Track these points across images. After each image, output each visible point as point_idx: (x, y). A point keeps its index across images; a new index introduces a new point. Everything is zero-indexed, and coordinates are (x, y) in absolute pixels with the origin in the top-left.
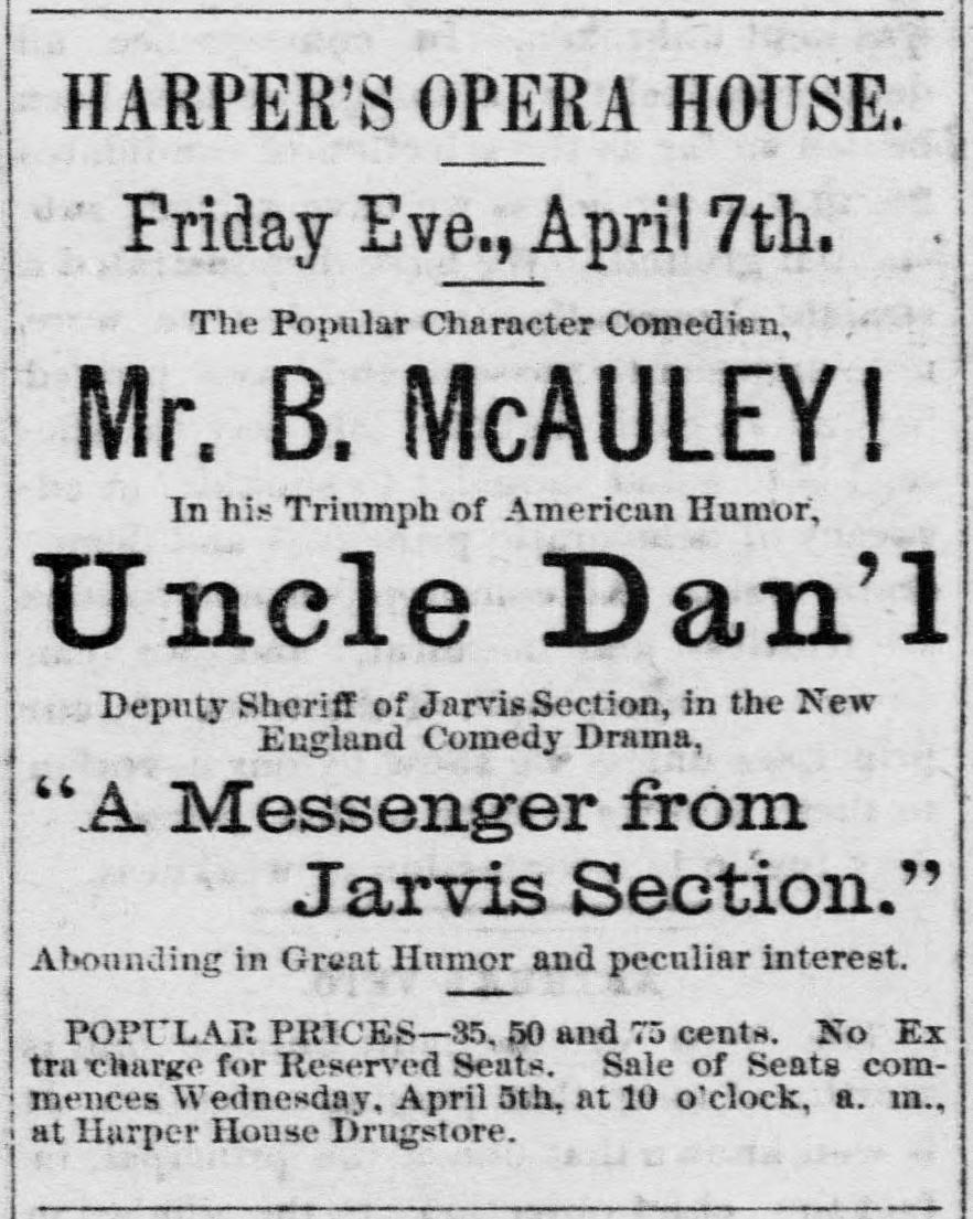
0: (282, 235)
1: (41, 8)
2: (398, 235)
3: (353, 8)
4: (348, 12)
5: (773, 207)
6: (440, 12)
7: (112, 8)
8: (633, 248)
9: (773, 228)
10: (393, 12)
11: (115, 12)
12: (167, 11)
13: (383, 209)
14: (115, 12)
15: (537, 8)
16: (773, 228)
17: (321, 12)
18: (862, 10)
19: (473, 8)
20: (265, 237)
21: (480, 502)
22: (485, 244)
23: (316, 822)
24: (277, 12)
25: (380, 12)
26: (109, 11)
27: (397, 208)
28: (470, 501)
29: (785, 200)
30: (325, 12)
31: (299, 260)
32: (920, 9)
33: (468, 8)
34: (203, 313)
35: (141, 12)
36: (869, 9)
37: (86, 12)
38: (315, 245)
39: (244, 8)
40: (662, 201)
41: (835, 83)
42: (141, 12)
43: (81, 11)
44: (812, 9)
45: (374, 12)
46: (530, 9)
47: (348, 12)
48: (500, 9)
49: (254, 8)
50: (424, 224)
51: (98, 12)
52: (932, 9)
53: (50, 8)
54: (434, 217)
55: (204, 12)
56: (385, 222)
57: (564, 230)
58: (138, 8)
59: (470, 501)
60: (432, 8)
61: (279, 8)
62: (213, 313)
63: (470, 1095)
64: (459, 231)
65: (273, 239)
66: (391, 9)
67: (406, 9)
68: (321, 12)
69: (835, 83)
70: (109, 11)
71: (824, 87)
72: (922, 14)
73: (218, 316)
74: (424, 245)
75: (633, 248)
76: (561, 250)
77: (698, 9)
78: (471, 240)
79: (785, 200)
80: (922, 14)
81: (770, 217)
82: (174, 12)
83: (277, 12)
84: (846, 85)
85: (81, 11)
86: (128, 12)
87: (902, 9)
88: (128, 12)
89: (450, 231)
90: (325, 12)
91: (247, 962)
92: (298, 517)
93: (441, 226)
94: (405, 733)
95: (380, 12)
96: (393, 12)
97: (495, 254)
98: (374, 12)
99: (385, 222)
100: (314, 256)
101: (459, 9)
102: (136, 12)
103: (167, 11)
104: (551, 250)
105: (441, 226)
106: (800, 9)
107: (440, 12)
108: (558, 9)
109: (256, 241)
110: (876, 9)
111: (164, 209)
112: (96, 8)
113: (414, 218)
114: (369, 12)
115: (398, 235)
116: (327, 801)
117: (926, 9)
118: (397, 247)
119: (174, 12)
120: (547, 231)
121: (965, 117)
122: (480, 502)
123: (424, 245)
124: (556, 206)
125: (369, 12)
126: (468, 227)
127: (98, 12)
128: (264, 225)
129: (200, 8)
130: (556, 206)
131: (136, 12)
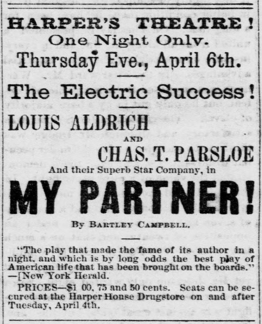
0: (85, 63)
1: (12, 319)
2: (116, 63)
3: (96, 319)
4: (95, 320)
5: (224, 56)
6: (119, 320)
7: (31, 319)
8: (183, 66)
9: (224, 61)
10: (107, 320)
11: (32, 320)
12: (46, 320)
13: (113, 56)
14: (32, 320)
15: (146, 319)
16: (224, 61)
17: (87, 320)
18: (233, 320)
19: (128, 319)
20: (80, 64)
21: (173, 248)
22: (140, 65)
23: (228, 96)
24: (75, 320)
25: (103, 320)
26: (30, 320)
27: (116, 56)
28: (170, 248)
29: (227, 54)
30: (89, 320)
31: (89, 70)
32: (248, 320)
33: (127, 319)
34: (27, 247)
35: (39, 320)
36: (235, 320)
37: (24, 320)
38: (93, 65)
39: (67, 319)
40: (191, 54)
41: (218, 148)
42: (39, 320)
43: (23, 320)
44: (220, 320)
45: (102, 320)
46: (144, 319)
47: (95, 320)
48: (135, 320)
49: (69, 319)
50: (123, 60)
51: (27, 320)
52: (252, 320)
53: (14, 319)
54: (126, 58)
55: (56, 320)
56: (113, 59)
57: (164, 62)
58: (38, 319)
59: (170, 248)
60: (117, 319)
61: (76, 319)
62: (29, 247)
63: (74, 304)
64: (133, 62)
65: (82, 64)
66: (106, 320)
67: (110, 319)
68: (87, 320)
69: (218, 148)
70: (30, 320)
71: (215, 150)
72: (249, 321)
73: (31, 248)
74: (123, 66)
75: (183, 66)
76: (163, 67)
77: (189, 320)
78: (136, 64)
79: (227, 54)
80: (249, 321)
81: (223, 58)
82: (48, 320)
83: (75, 320)
84: (220, 149)
85: (23, 320)
86: (35, 320)
87: (244, 320)
88: (35, 320)
89: (130, 62)
90: (89, 320)
91: (210, 171)
92: (12, 308)
93: (128, 60)
94: (56, 257)
95: (103, 320)
96: (107, 320)
97: (143, 67)
98: (102, 320)
99: (113, 59)
100: (93, 68)
101: (124, 319)
102: (37, 320)
103: (46, 320)
104: (160, 67)
105: (128, 60)
106: (216, 320)
107: (119, 320)
108: (151, 320)
109: (77, 64)
110: (237, 320)
111: (116, 56)
112: (27, 319)
113: (121, 58)
114: (100, 320)
115: (116, 63)
116: (231, 90)
117: (250, 320)
118: (116, 66)
119: (48, 320)
120: (159, 62)
121: (228, 5)
122: (173, 248)
123: (123, 66)
124: (162, 54)
125: (100, 320)
126: (135, 61)
127: (27, 320)
128: (80, 60)
129: (55, 319)
130: (162, 54)
131: (37, 320)
